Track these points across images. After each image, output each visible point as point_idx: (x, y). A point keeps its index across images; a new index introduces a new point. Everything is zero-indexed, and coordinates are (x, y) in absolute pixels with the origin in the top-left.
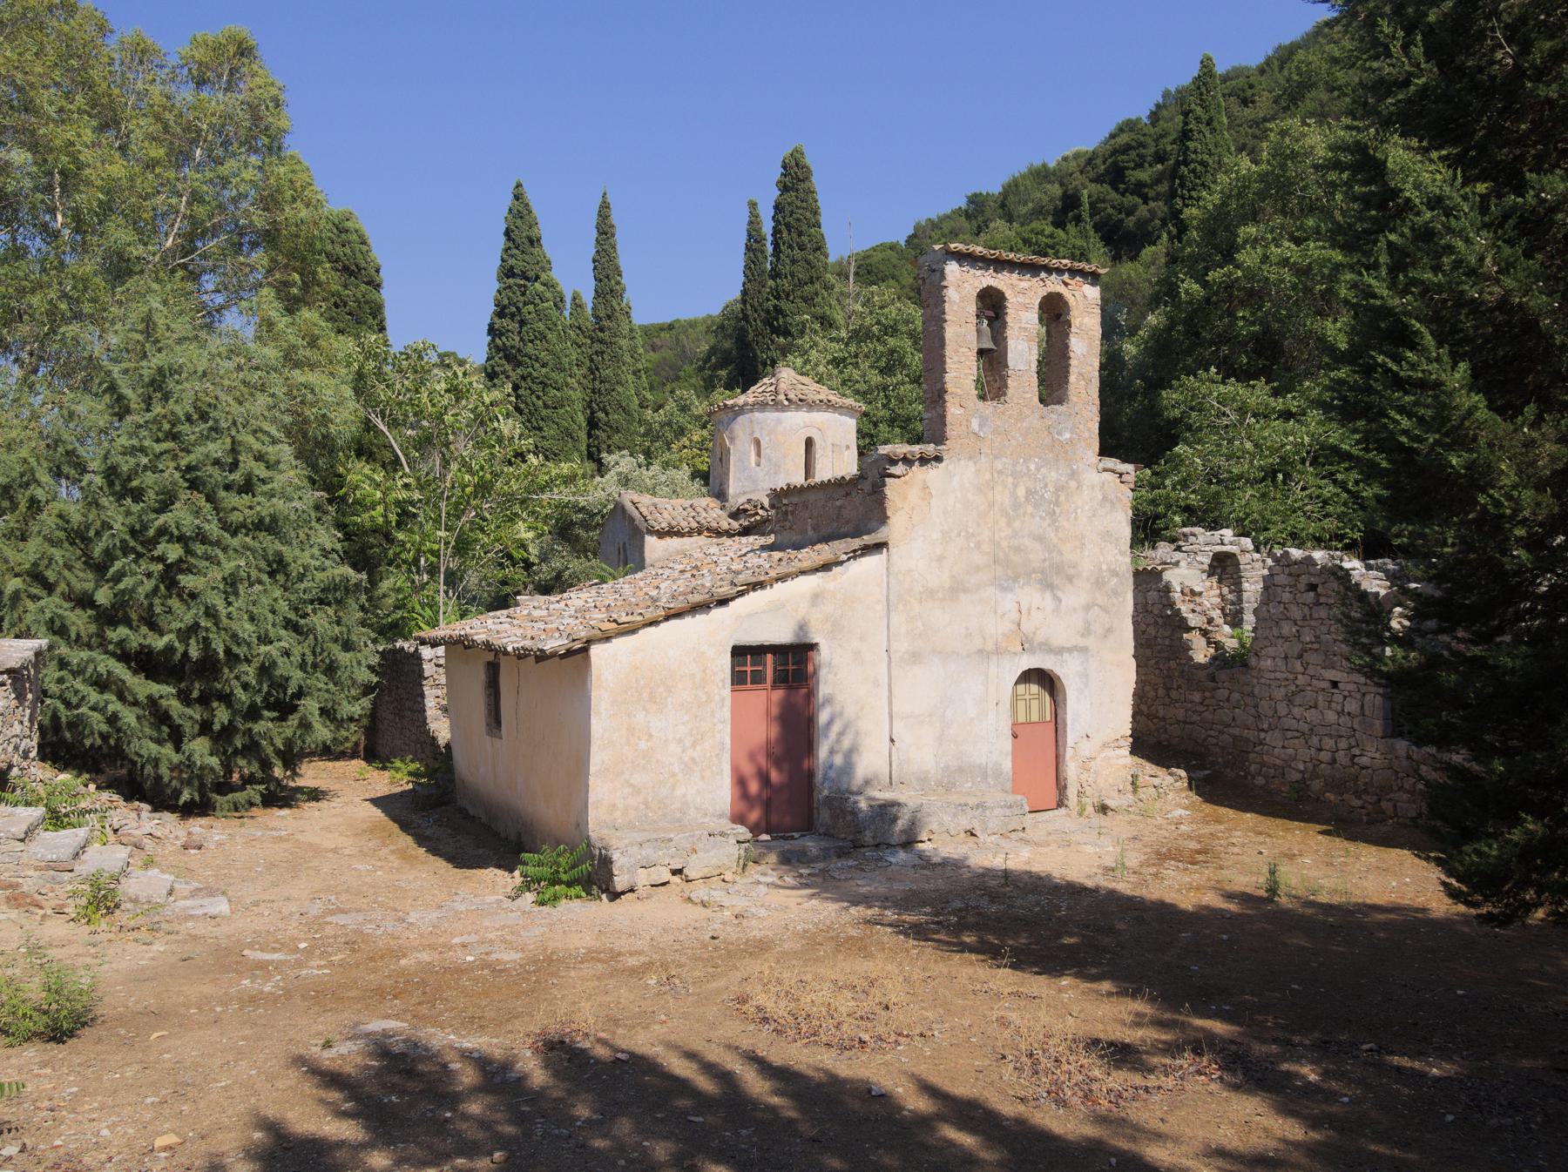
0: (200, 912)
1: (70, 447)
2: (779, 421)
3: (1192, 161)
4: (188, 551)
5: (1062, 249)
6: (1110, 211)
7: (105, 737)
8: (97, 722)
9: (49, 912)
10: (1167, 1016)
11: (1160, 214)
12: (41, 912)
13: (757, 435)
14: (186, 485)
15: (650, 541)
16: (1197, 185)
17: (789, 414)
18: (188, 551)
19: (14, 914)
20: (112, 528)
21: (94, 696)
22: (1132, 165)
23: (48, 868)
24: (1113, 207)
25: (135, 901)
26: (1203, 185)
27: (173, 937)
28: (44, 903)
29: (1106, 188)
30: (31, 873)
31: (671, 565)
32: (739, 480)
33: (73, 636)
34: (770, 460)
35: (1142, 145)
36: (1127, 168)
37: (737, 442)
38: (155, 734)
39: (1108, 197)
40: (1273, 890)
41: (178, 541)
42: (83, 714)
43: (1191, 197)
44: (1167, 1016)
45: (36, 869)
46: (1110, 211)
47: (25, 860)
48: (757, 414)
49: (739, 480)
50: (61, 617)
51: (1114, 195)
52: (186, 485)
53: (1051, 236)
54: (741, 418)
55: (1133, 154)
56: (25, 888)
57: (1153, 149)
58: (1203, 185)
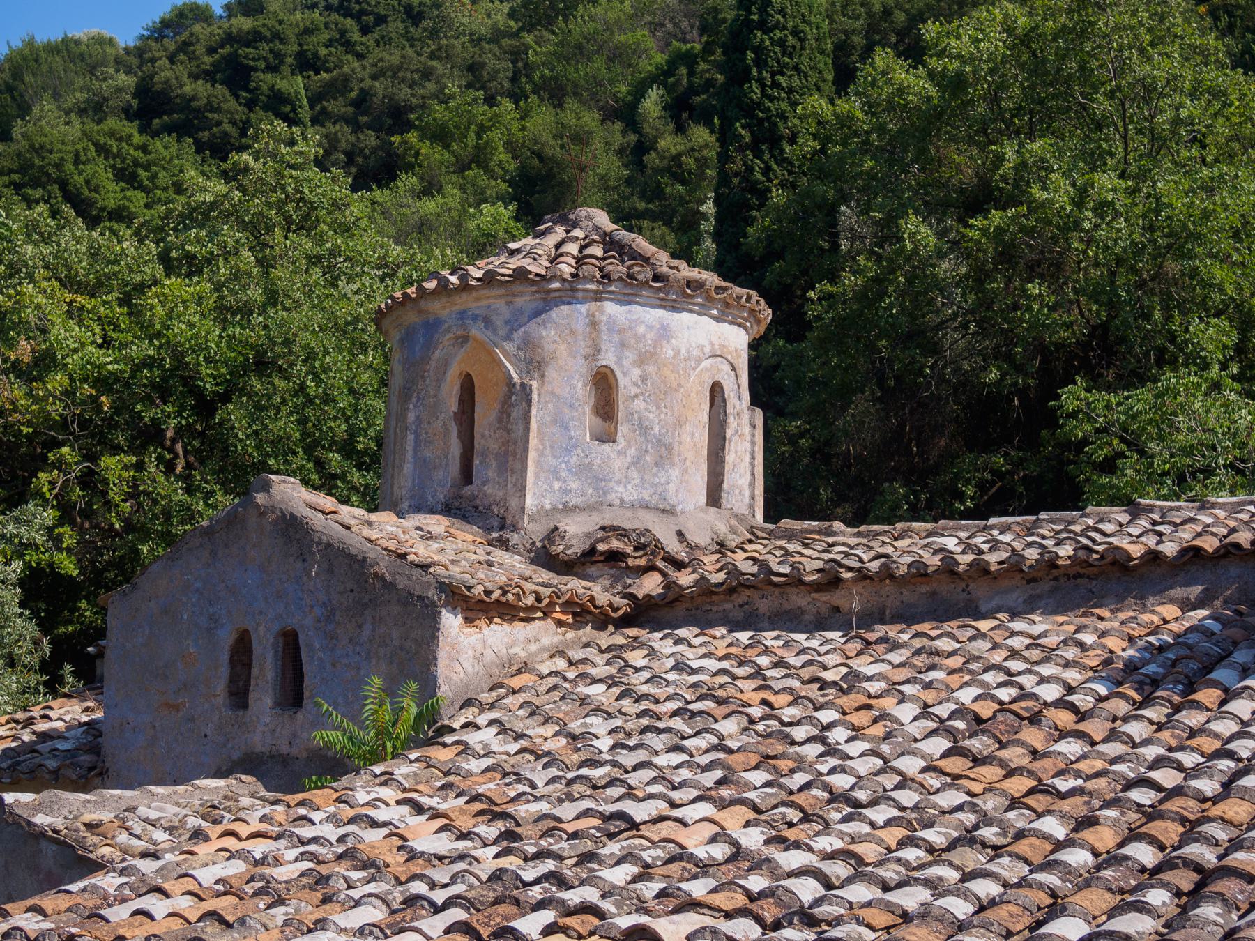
2: (665, 333)
3: (777, 26)
5: (162, 174)
6: (227, 127)
11: (343, 145)
13: (608, 359)
15: (451, 622)
16: (786, 66)
17: (685, 317)
20: (1063, 140)
22: (262, 65)
24: (233, 122)
26: (796, 68)
29: (221, 90)
31: (813, 691)
32: (555, 472)
34: (644, 429)
35: (278, 37)
36: (255, 69)
37: (551, 373)
39: (225, 106)
43: (776, 85)
46: (227, 127)
48: (610, 308)
49: (555, 472)
51: (232, 104)
53: (144, 148)
54: (560, 313)
55: (264, 49)
57: (295, 48)
58: (796, 68)
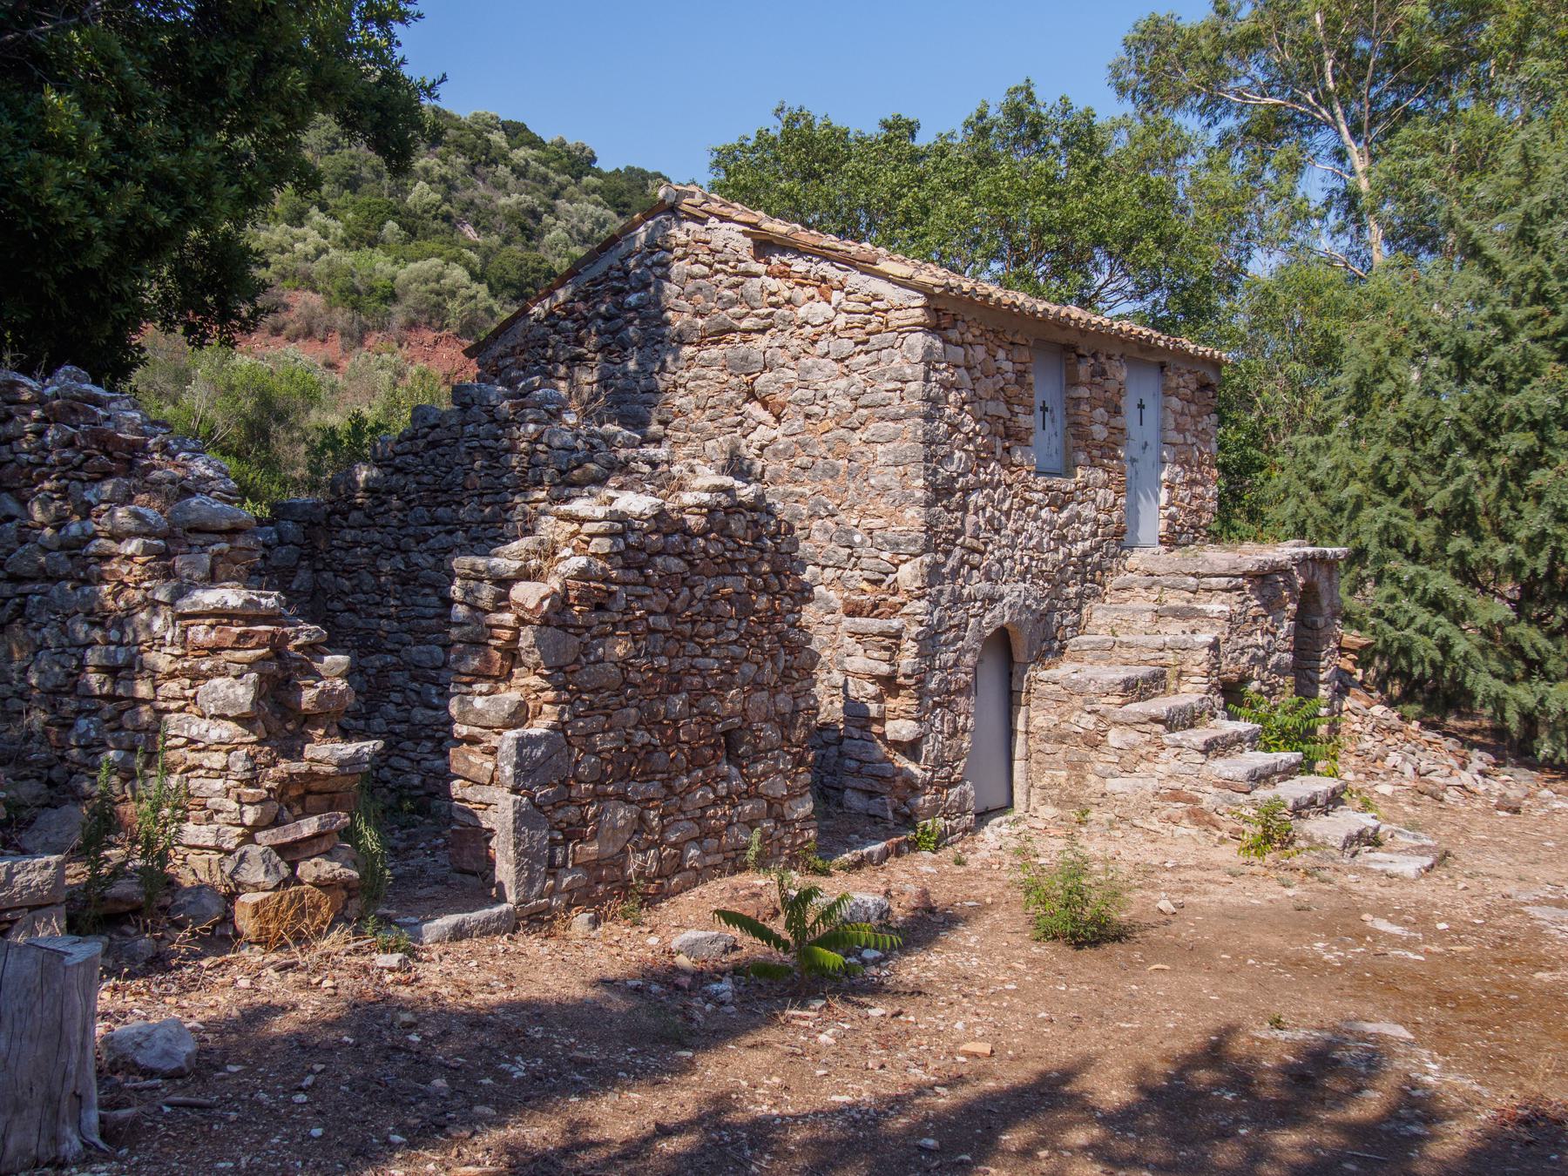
0: (1378, 867)
1: (1424, 328)
4: (1544, 440)
7: (1438, 669)
8: (1426, 648)
9: (1226, 835)
10: (220, 960)
12: (1219, 834)
14: (1555, 356)
18: (1544, 440)
19: (1194, 831)
21: (1423, 617)
23: (1225, 786)
25: (1310, 839)
27: (1326, 887)
28: (1222, 825)
30: (1210, 789)
33: (1410, 547)
38: (1501, 669)
40: (430, 90)
41: (1532, 429)
42: (1407, 637)
44: (220, 960)
45: (1215, 785)
47: (1204, 773)
50: (1396, 527)
52: (1555, 356)
56: (1204, 805)
